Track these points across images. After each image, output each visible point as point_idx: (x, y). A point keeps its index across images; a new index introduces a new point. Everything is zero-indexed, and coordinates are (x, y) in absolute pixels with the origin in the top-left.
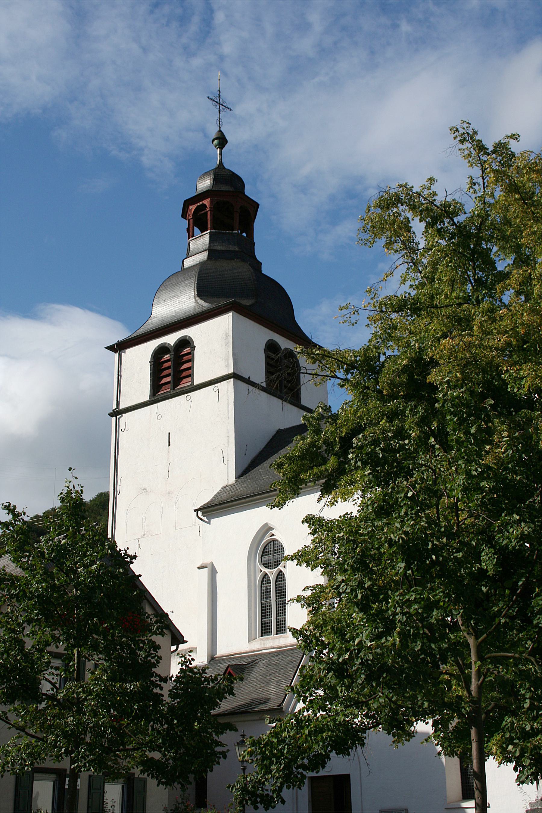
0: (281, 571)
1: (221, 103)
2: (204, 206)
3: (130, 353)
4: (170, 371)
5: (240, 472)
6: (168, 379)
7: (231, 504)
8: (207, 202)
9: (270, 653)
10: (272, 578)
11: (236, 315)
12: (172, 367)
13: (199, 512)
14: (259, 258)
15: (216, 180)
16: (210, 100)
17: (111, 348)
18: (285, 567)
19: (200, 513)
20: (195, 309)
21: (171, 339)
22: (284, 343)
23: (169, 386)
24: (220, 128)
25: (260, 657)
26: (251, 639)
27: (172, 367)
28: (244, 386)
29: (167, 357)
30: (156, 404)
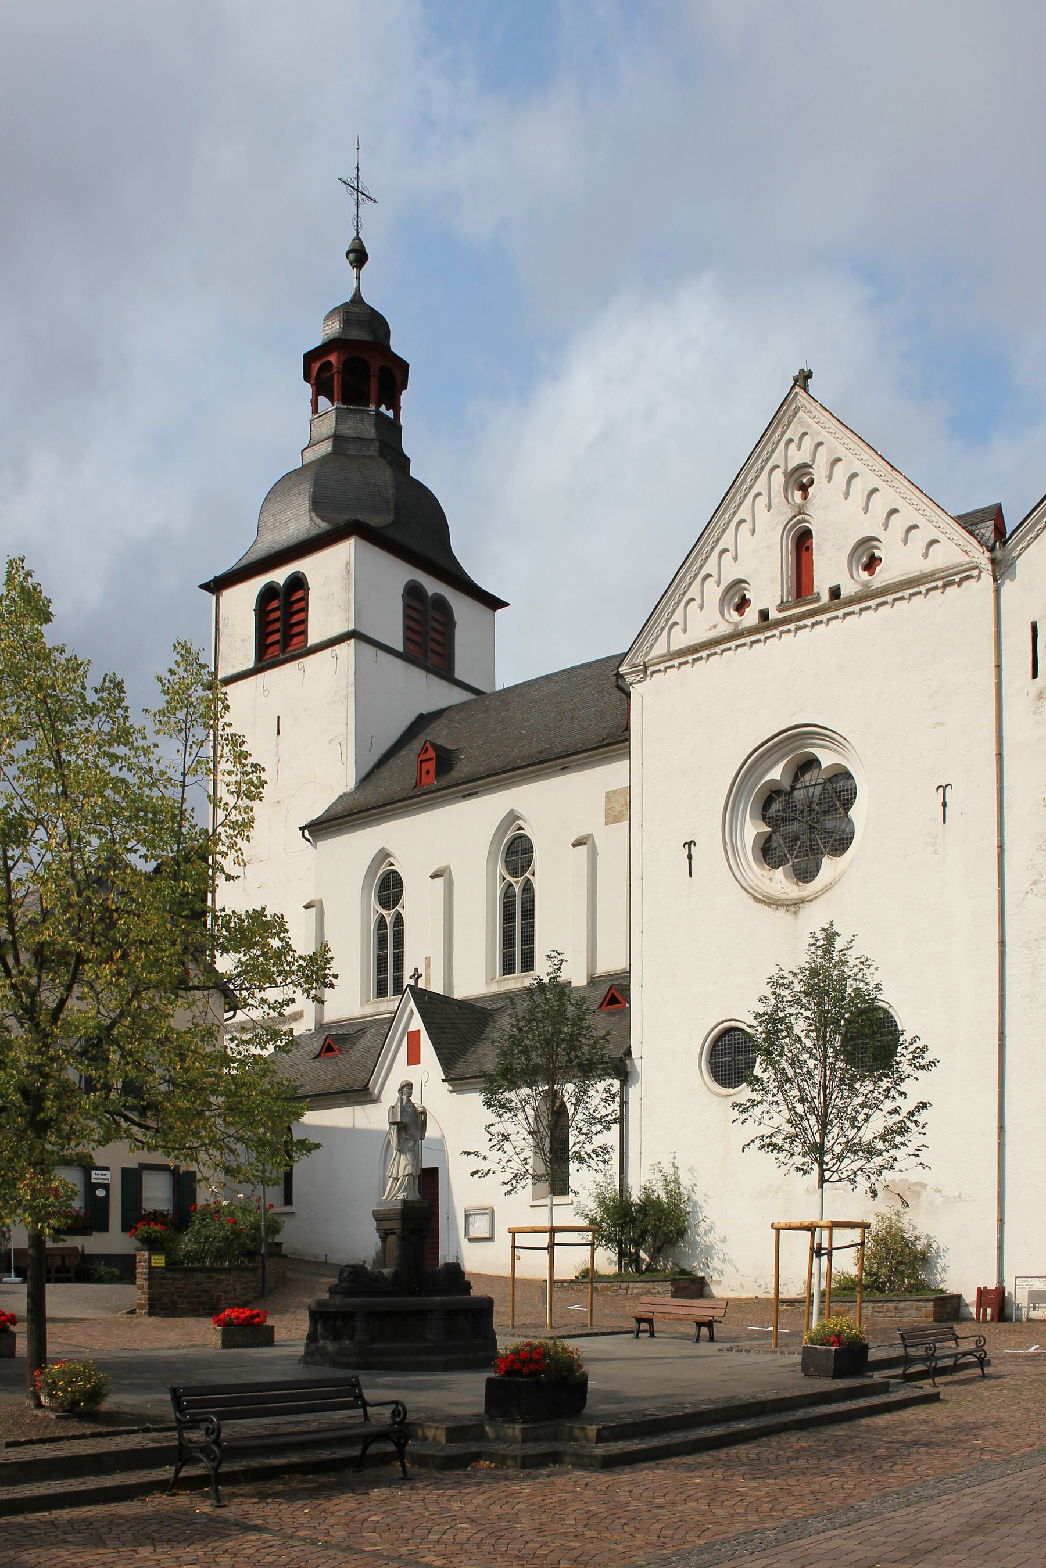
0: (529, 880)
1: (360, 189)
2: (329, 363)
3: (229, 595)
4: (278, 625)
5: (364, 773)
6: (276, 637)
7: (341, 820)
8: (333, 358)
9: (383, 1019)
10: (517, 889)
11: (361, 541)
12: (281, 619)
13: (306, 831)
14: (407, 452)
15: (347, 323)
16: (343, 184)
17: (205, 587)
18: (533, 874)
19: (306, 831)
20: (309, 530)
21: (280, 576)
22: (432, 586)
23: (277, 647)
24: (358, 233)
25: (371, 1024)
26: (365, 1001)
27: (281, 619)
28: (369, 650)
29: (275, 604)
30: (262, 674)
